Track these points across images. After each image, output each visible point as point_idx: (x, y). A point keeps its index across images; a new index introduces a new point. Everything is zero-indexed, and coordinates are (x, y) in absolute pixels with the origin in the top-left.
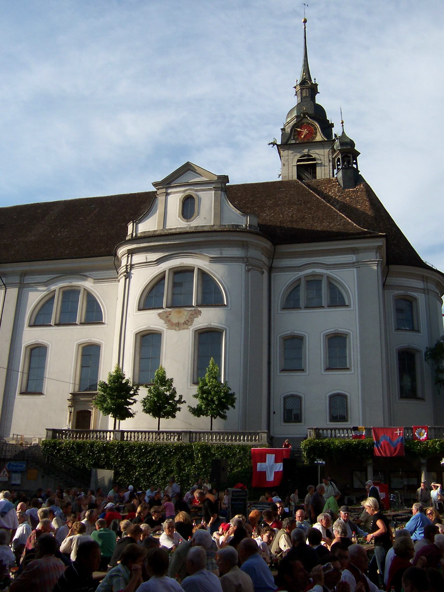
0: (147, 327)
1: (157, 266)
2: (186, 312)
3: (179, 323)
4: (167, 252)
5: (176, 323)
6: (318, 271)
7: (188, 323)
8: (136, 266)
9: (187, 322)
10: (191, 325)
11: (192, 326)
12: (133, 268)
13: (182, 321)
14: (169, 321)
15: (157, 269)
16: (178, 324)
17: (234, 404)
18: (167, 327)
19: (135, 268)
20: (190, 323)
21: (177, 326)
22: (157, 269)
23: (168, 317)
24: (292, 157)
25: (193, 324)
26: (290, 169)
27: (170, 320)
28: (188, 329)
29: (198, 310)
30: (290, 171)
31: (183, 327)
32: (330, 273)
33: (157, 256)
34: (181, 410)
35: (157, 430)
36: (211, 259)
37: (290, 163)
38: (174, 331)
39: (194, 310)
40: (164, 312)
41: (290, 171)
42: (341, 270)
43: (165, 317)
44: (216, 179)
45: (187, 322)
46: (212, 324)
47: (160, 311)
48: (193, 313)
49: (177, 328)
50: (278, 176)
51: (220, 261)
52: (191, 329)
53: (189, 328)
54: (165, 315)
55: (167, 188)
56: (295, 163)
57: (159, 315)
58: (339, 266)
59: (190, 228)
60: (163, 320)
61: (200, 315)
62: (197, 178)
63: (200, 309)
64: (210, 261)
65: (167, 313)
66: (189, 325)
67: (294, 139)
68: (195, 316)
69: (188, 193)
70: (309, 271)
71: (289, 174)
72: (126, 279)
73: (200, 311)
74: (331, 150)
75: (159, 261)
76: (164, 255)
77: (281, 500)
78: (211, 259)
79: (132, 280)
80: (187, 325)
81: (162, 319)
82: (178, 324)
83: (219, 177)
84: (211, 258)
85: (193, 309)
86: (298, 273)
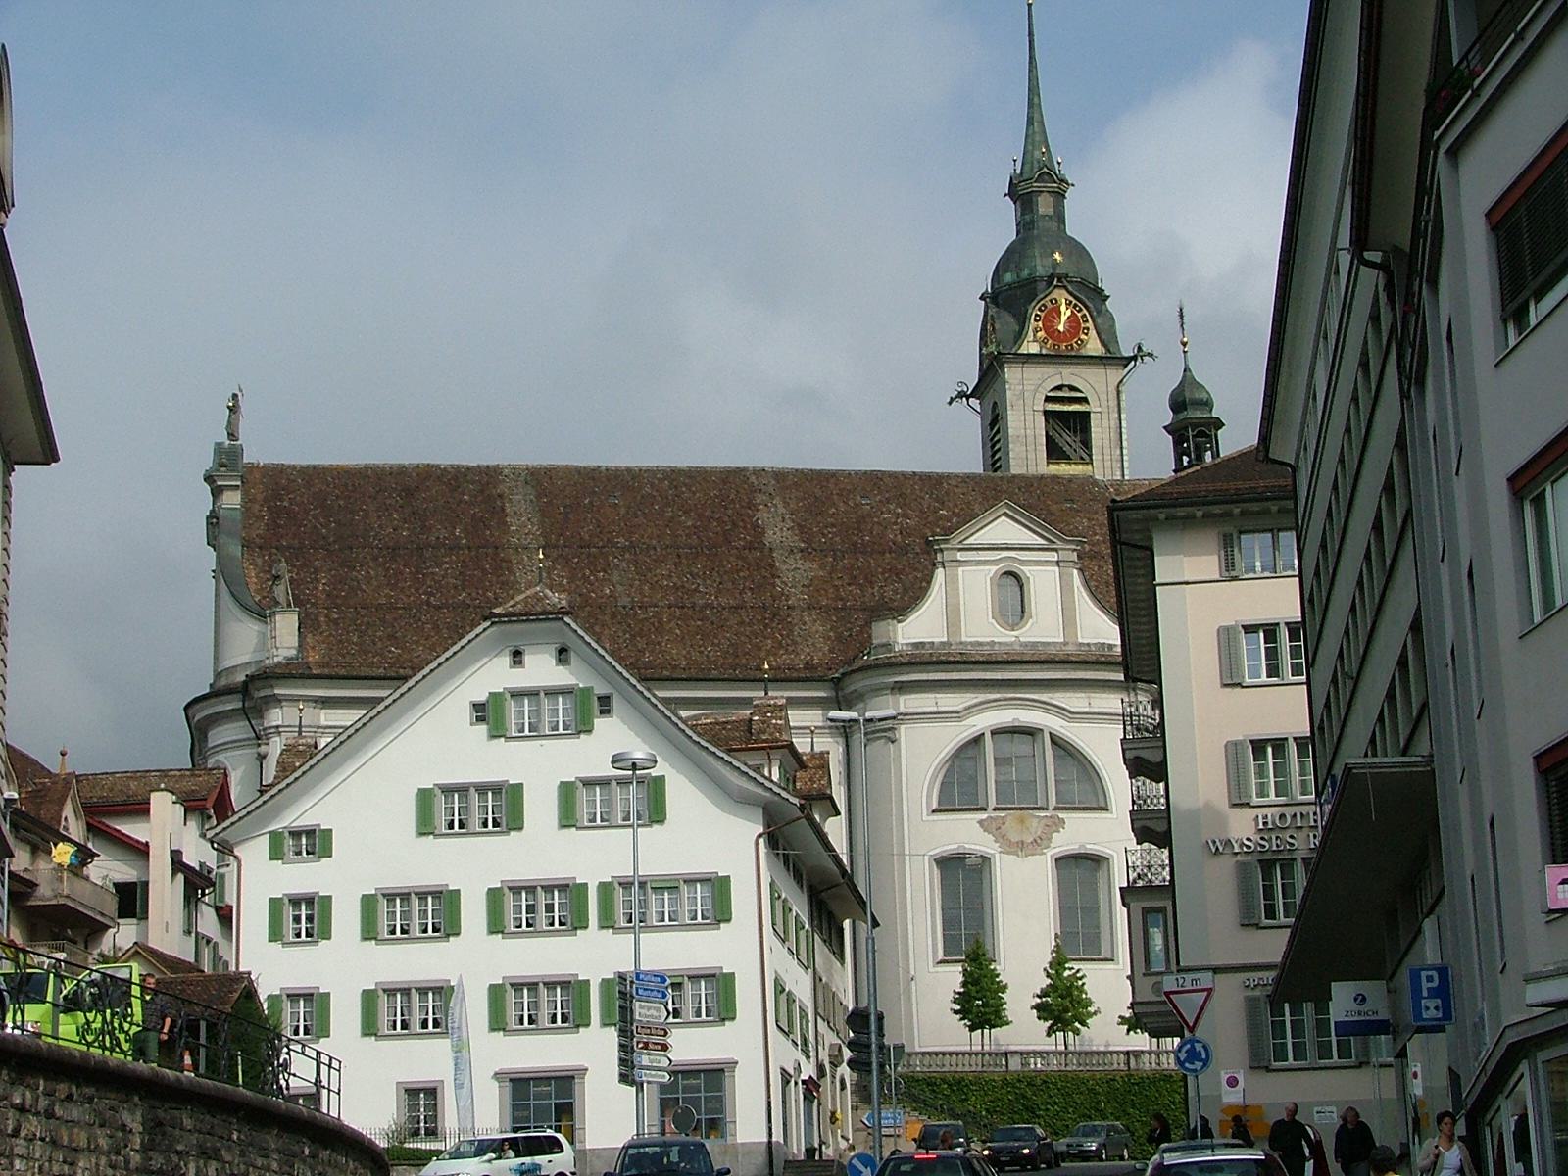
2: (1036, 821)
3: (1023, 842)
5: (1017, 842)
7: (1039, 843)
16: (1022, 844)
17: (1539, 1053)
18: (999, 849)
21: (1020, 848)
24: (1033, 388)
26: (1030, 418)
27: (1005, 835)
30: (1029, 424)
34: (1118, 1020)
35: (980, 1047)
37: (1029, 402)
41: (1029, 424)
47: (983, 816)
50: (948, 400)
52: (1049, 854)
53: (1045, 853)
56: (1040, 405)
57: (981, 822)
59: (1022, 644)
63: (1062, 815)
67: (1036, 341)
71: (1028, 431)
73: (1063, 819)
76: (975, 701)
77: (1397, 1156)
82: (1022, 844)
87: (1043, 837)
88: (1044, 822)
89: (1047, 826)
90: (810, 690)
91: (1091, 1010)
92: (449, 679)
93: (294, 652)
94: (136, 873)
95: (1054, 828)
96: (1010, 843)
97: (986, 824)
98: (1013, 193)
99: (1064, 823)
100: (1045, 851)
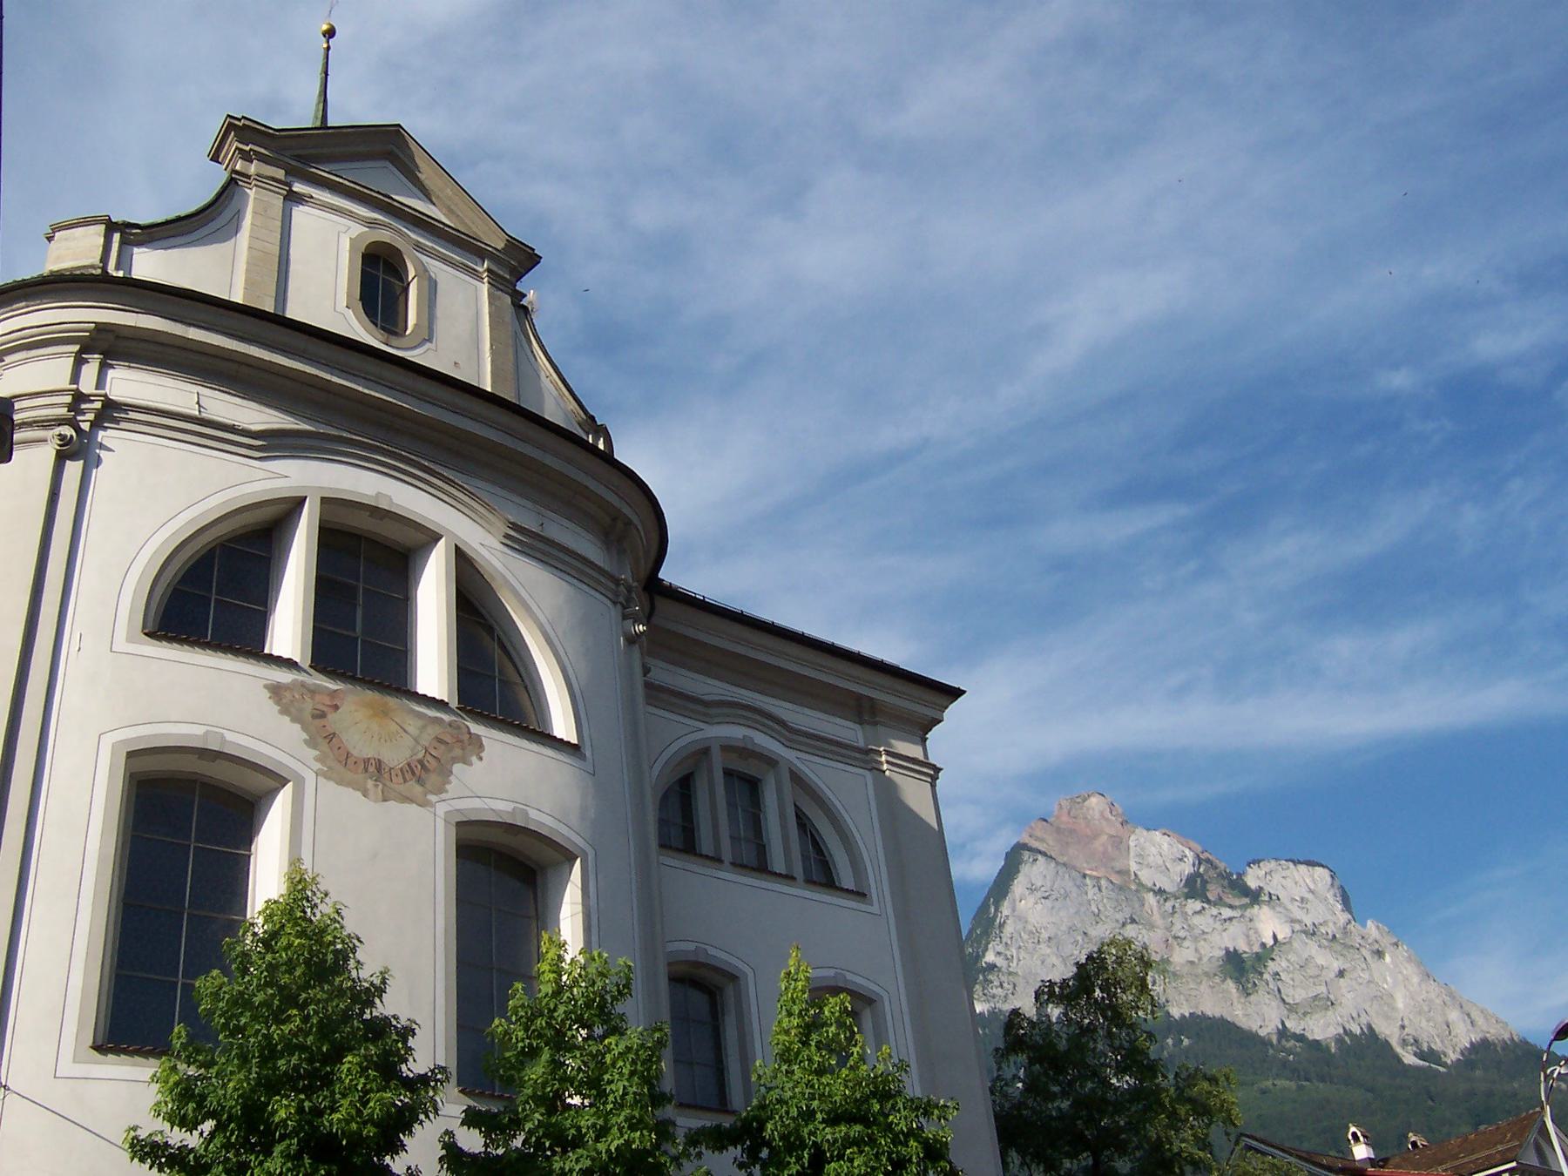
0: (207, 732)
1: (260, 459)
4: (307, 419)
5: (367, 761)
6: (765, 742)
8: (132, 415)
9: (418, 770)
10: (440, 790)
11: (444, 796)
12: (117, 421)
13: (395, 756)
14: (331, 737)
15: (262, 474)
16: (376, 769)
18: (317, 766)
19: (123, 425)
20: (433, 779)
22: (262, 474)
23: (323, 715)
25: (448, 787)
28: (424, 804)
29: (470, 733)
31: (398, 785)
32: (796, 762)
33: (264, 418)
36: (512, 533)
38: (359, 794)
39: (450, 724)
40: (303, 685)
42: (825, 762)
43: (307, 715)
44: (500, 245)
45: (418, 770)
46: (533, 814)
48: (447, 738)
49: (370, 784)
51: (538, 555)
52: (442, 809)
53: (432, 805)
54: (308, 706)
55: (295, 173)
57: (276, 690)
58: (826, 746)
60: (297, 727)
61: (481, 759)
62: (413, 197)
64: (507, 536)
65: (318, 697)
66: (428, 786)
68: (457, 752)
69: (384, 236)
70: (736, 732)
72: (61, 458)
74: (93, 325)
75: (273, 444)
78: (512, 533)
79: (98, 475)
80: (420, 781)
81: (294, 720)
82: (376, 769)
83: (514, 246)
84: (514, 526)
85: (446, 717)
86: (702, 725)
87: (432, 764)
88: (433, 731)
89: (440, 741)
90: (351, 381)
91: (136, 1160)
92: (120, 948)
93: (99, 440)
94: (1125, 1172)
95: (457, 752)
96: (346, 758)
97: (288, 695)
98: (1036, 993)
99: (481, 746)
100: (433, 798)
